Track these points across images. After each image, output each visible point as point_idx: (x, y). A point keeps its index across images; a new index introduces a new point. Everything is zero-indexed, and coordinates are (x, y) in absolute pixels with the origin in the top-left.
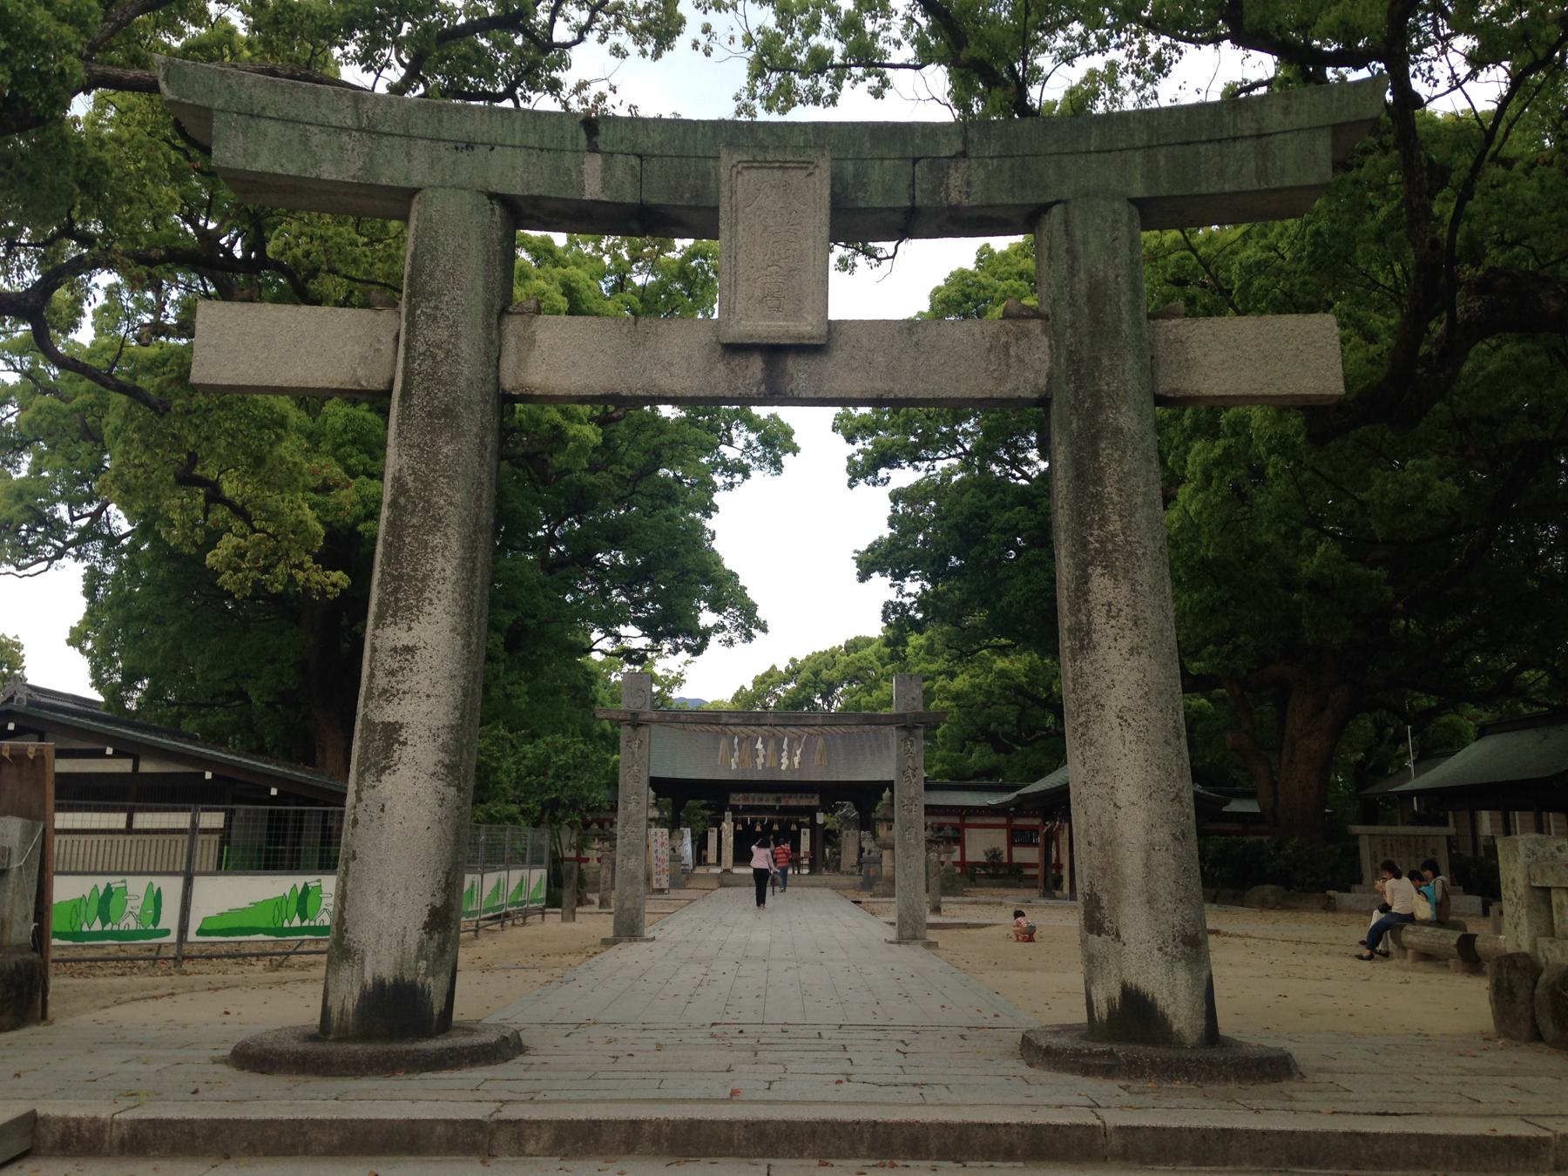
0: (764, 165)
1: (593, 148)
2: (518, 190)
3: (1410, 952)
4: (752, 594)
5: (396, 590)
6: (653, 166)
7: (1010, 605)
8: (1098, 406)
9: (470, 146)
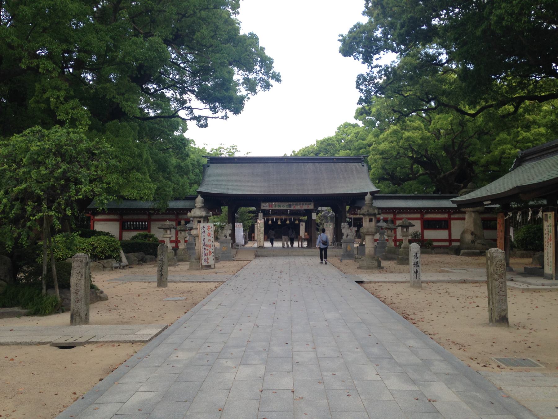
4: (268, 53)
7: (501, 18)
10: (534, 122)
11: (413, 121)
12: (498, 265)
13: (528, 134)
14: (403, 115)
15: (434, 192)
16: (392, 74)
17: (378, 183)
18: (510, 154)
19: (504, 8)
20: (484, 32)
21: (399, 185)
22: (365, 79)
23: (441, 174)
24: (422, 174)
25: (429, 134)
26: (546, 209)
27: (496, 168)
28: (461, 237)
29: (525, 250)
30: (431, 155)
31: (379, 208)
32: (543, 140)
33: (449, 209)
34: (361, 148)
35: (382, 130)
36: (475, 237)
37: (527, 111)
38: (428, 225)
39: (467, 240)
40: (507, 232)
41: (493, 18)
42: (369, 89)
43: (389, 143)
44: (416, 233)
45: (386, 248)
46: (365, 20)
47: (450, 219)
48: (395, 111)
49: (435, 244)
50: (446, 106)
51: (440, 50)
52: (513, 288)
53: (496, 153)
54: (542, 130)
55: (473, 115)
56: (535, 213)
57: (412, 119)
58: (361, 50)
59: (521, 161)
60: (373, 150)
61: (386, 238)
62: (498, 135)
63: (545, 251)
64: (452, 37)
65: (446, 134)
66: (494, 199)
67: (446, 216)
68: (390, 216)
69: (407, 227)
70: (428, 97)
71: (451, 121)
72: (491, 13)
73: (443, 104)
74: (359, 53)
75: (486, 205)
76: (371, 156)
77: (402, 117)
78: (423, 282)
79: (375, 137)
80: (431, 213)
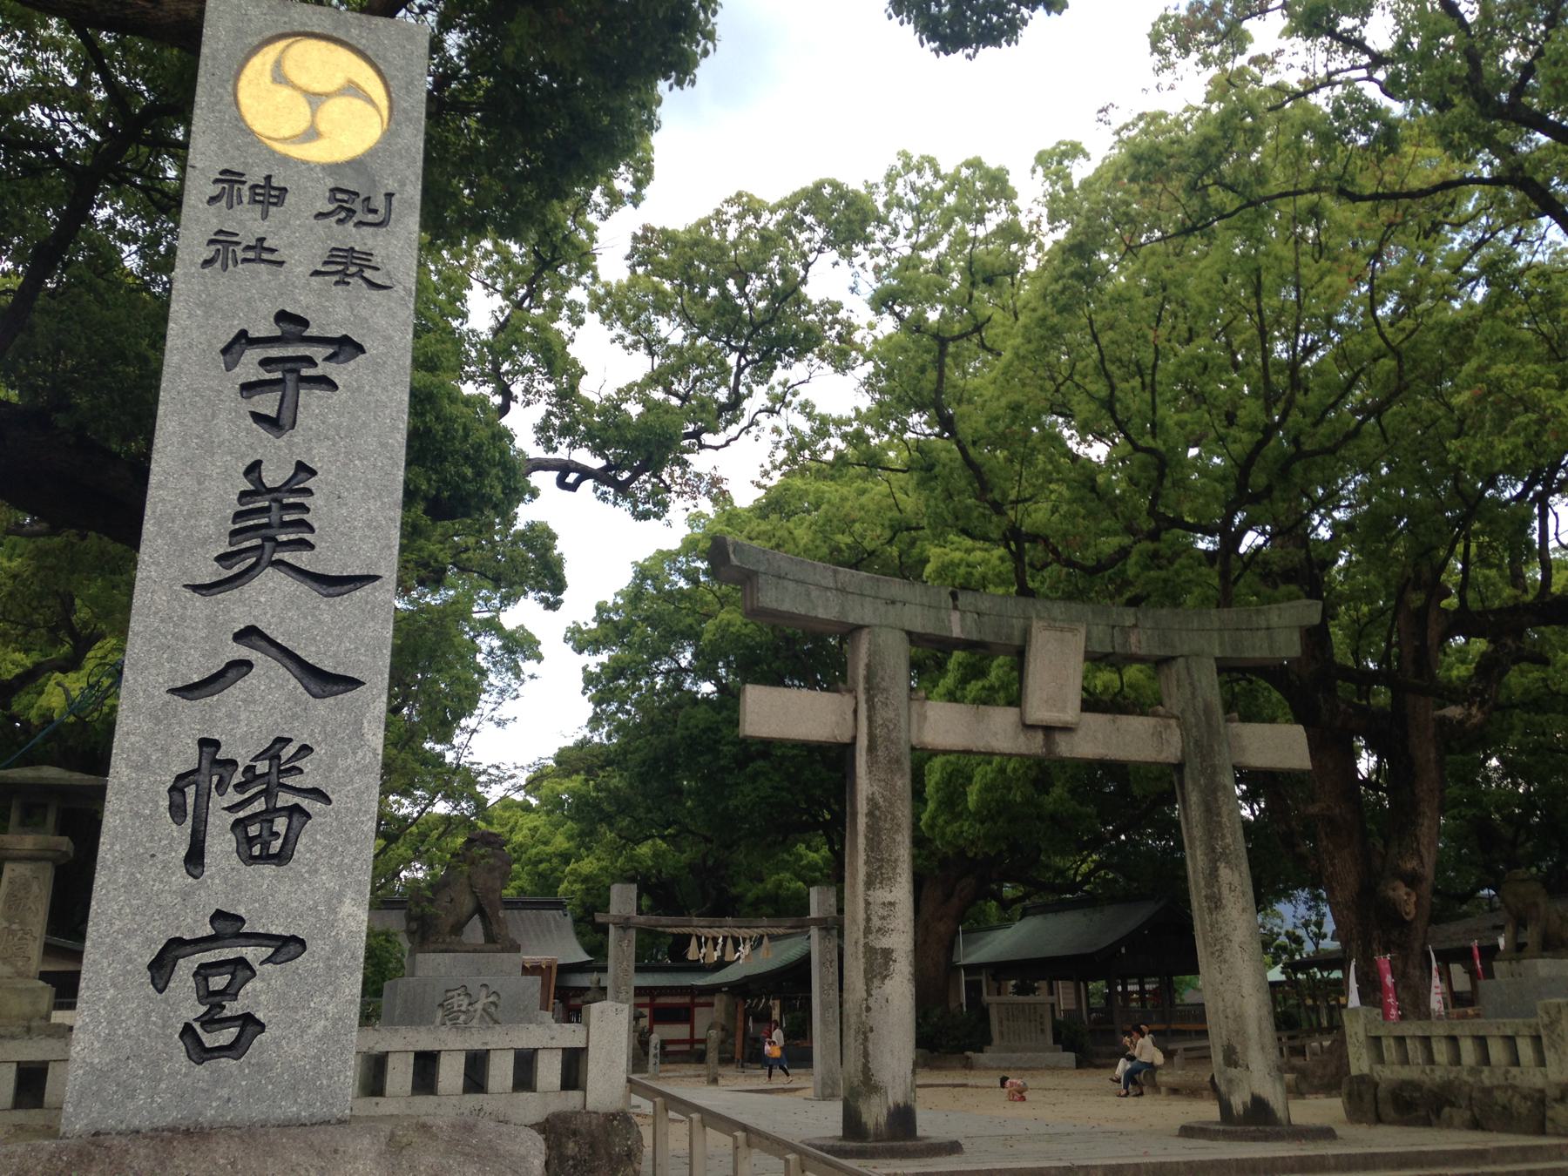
0: (1055, 629)
1: (955, 608)
2: (919, 630)
3: (1163, 1089)
5: (880, 868)
6: (986, 619)
8: (1214, 773)
9: (893, 602)
34: (541, 861)
47: (693, 1005)
67: (687, 1000)
80: (666, 995)
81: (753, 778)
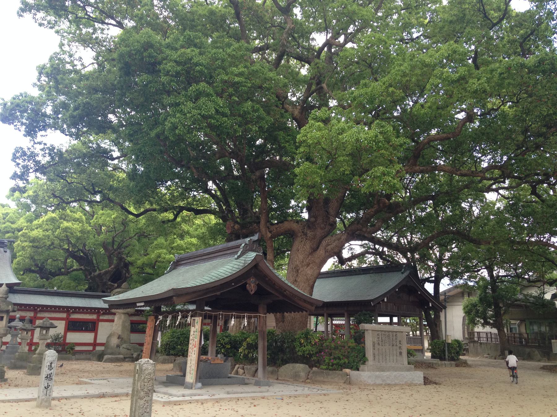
10: (188, 233)
11: (74, 212)
12: (146, 380)
13: (182, 242)
14: (64, 202)
15: (86, 290)
16: (59, 158)
17: (23, 274)
18: (164, 258)
19: (178, 118)
20: (158, 136)
21: (47, 279)
22: (24, 154)
23: (96, 271)
24: (76, 270)
25: (89, 228)
26: (194, 314)
27: (150, 271)
28: (107, 341)
29: (167, 355)
30: (89, 251)
31: (15, 304)
32: (194, 250)
33: (99, 309)
34: (8, 232)
35: (38, 216)
36: (121, 341)
37: (184, 220)
38: (74, 326)
39: (112, 345)
40: (155, 337)
41: (168, 125)
42: (27, 166)
43: (44, 231)
44: (58, 335)
45: (17, 354)
46: (35, 93)
47: (99, 320)
48: (55, 196)
49: (77, 348)
50: (111, 201)
51: (112, 148)
52: (157, 401)
53: (152, 256)
54: (194, 241)
55: (137, 216)
56: (185, 317)
57: (75, 210)
58: (24, 121)
59: (177, 264)
60: (22, 235)
61: (19, 340)
62: (156, 239)
63: (189, 358)
64: (127, 132)
65: (107, 231)
66: (149, 301)
67: (94, 317)
68: (30, 314)
69: (47, 328)
70: (94, 189)
71: (114, 218)
72: (165, 119)
73: (108, 199)
74: (22, 124)
75: (139, 307)
76: (19, 242)
77: (62, 204)
78: (53, 399)
79: (27, 222)
81: (198, 95)
